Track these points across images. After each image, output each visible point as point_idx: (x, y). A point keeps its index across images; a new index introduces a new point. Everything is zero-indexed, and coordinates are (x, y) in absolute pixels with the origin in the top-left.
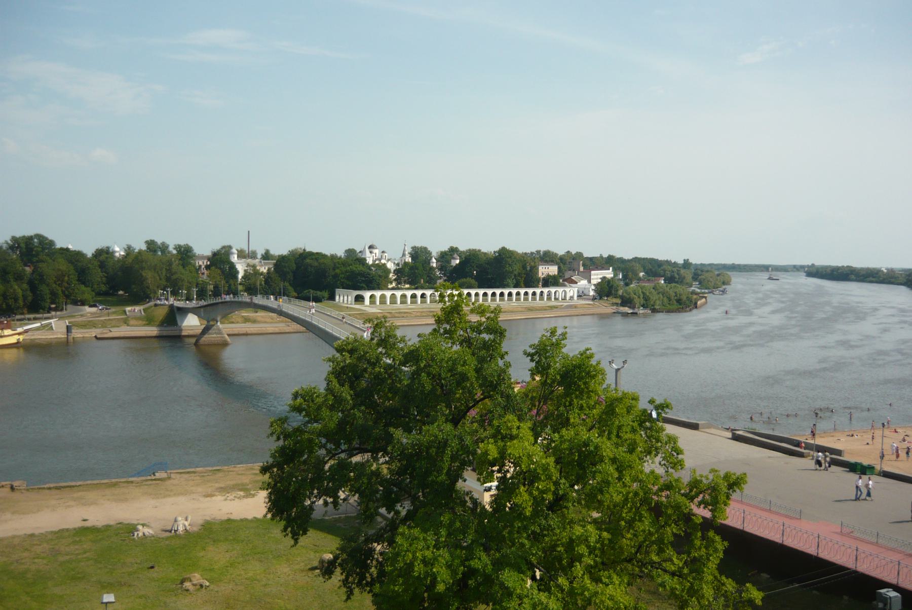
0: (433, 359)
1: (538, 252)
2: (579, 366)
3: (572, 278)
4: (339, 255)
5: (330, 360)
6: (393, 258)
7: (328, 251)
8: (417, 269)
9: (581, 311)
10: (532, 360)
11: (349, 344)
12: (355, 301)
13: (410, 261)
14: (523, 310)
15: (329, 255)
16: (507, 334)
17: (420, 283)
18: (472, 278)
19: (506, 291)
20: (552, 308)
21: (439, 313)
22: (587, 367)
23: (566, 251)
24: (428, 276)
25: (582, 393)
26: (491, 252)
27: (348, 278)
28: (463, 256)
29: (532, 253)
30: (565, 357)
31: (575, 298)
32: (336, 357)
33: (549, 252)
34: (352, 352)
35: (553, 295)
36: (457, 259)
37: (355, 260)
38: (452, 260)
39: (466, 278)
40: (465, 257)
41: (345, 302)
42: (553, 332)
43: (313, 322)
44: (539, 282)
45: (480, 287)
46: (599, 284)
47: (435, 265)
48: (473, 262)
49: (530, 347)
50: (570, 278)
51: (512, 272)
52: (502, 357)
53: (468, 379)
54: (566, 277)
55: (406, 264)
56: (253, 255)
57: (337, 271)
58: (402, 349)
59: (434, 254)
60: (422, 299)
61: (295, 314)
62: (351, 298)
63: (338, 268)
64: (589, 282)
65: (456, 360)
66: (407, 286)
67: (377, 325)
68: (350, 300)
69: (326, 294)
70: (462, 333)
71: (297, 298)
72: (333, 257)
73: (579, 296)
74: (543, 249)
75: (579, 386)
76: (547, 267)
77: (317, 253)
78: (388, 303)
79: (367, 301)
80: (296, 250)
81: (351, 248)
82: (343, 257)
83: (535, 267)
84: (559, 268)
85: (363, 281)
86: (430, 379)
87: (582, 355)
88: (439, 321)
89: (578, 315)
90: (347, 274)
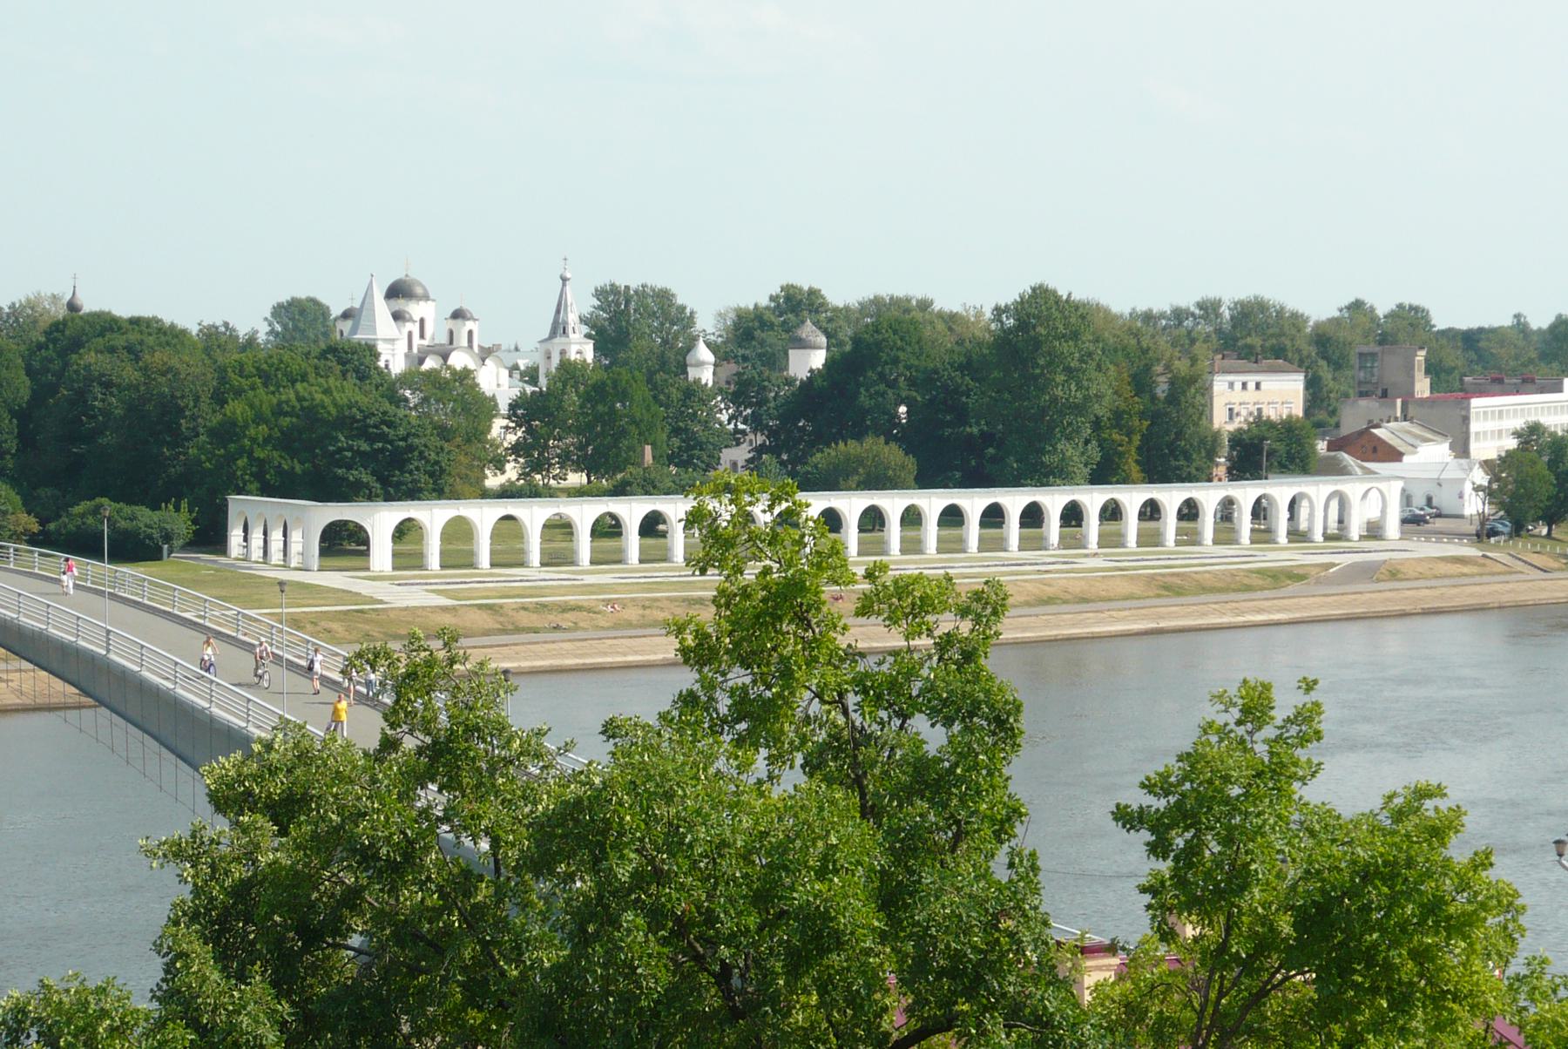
0: (674, 842)
1: (1209, 308)
2: (1386, 872)
3: (1375, 431)
4: (243, 331)
5: (177, 852)
6: (507, 343)
7: (188, 316)
8: (624, 396)
9: (1427, 596)
10: (1158, 848)
11: (273, 771)
12: (324, 552)
13: (589, 355)
14: (1136, 589)
15: (194, 330)
16: (1025, 722)
17: (639, 464)
18: (889, 439)
19: (1053, 501)
20: (1279, 578)
21: (707, 615)
22: (1428, 874)
24: (676, 431)
25: (1402, 1003)
26: (979, 314)
27: (287, 442)
28: (846, 333)
29: (1179, 315)
30: (1324, 826)
31: (1393, 528)
32: (209, 833)
34: (284, 811)
35: (1284, 515)
36: (816, 347)
37: (323, 355)
38: (793, 354)
39: (859, 436)
40: (856, 341)
41: (276, 556)
42: (1255, 708)
43: (113, 656)
44: (1211, 455)
45: (926, 481)
46: (1508, 460)
47: (707, 376)
48: (896, 361)
49: (1148, 786)
50: (1365, 433)
51: (1079, 409)
52: (1002, 829)
53: (838, 941)
54: (1345, 430)
55: (569, 371)
57: (237, 408)
58: (530, 796)
59: (708, 323)
60: (650, 541)
61: (27, 621)
62: (305, 540)
63: (239, 393)
64: (1461, 449)
65: (782, 848)
66: (576, 479)
67: (411, 675)
68: (296, 546)
69: (179, 521)
70: (816, 708)
71: (34, 540)
72: (215, 340)
73: (1412, 521)
74: (1231, 290)
75: (1388, 968)
76: (1251, 379)
77: (135, 321)
78: (484, 559)
80: (31, 304)
81: (302, 294)
82: (262, 337)
83: (1192, 380)
84: (1312, 385)
85: (358, 453)
86: (664, 942)
87: (1399, 815)
88: (699, 654)
89: (1404, 615)
90: (286, 421)
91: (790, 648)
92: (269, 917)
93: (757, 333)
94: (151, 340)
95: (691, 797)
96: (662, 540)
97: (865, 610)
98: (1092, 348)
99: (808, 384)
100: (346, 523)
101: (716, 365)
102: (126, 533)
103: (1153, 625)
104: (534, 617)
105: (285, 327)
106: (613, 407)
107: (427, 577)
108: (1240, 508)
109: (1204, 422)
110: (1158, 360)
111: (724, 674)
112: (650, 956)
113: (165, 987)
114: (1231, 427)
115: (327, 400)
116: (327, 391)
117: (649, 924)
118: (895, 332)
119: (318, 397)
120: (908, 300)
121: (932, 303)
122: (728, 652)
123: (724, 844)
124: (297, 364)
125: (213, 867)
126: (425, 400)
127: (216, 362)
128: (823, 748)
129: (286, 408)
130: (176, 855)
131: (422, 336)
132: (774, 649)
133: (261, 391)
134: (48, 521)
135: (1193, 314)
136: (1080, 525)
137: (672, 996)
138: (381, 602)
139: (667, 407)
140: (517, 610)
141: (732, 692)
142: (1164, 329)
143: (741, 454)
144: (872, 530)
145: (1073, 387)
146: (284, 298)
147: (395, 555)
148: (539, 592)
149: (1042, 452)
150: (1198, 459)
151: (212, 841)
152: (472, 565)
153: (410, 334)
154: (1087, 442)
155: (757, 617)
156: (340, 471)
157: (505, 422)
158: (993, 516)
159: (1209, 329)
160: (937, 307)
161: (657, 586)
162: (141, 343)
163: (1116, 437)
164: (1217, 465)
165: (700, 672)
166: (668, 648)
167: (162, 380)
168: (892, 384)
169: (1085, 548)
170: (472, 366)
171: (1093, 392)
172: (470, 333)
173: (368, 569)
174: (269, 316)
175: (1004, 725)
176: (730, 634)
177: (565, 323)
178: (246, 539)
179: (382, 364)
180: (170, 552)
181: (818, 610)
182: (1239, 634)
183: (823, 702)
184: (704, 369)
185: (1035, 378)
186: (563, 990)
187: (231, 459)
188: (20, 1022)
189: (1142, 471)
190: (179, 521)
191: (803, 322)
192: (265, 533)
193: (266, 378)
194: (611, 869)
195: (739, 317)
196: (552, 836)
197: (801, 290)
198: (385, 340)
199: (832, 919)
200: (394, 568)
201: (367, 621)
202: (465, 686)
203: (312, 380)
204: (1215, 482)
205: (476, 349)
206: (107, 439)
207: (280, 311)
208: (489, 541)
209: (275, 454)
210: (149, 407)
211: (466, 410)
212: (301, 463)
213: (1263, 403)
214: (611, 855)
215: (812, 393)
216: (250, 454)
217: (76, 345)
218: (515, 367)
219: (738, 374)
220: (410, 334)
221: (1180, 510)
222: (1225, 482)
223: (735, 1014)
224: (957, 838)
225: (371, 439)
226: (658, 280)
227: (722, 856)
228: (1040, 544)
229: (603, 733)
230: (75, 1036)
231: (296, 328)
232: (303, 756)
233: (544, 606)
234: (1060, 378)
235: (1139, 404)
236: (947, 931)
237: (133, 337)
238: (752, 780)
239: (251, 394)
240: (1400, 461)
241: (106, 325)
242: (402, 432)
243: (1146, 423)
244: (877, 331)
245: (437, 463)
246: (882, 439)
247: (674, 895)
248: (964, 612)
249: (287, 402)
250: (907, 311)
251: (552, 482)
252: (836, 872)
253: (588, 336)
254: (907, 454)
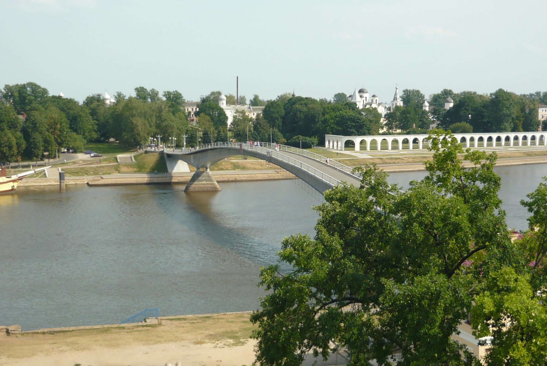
0: (425, 208)
1: (538, 94)
4: (328, 100)
5: (320, 209)
6: (384, 102)
8: (409, 113)
10: (530, 210)
12: (345, 147)
14: (521, 155)
16: (501, 182)
19: (503, 136)
26: (487, 95)
27: (337, 123)
28: (458, 99)
29: (531, 95)
32: (326, 205)
34: (342, 200)
36: (451, 102)
37: (345, 105)
38: (446, 104)
39: (460, 122)
40: (460, 101)
41: (335, 148)
43: (302, 168)
44: (538, 126)
45: (475, 131)
47: (427, 109)
49: (528, 196)
51: (509, 116)
52: (497, 206)
55: (397, 108)
57: (327, 116)
62: (341, 144)
63: (328, 113)
66: (399, 131)
67: (366, 173)
68: (339, 146)
69: (315, 140)
70: (455, 180)
71: (285, 144)
72: (323, 102)
77: (306, 98)
78: (379, 148)
80: (285, 95)
82: (332, 101)
83: (534, 109)
85: (352, 125)
88: (430, 168)
90: (337, 119)
91: (449, 167)
92: (338, 222)
93: (438, 99)
94: (309, 102)
95: (428, 199)
96: (417, 144)
97: (466, 158)
98: (512, 102)
99: (449, 111)
100: (350, 140)
101: (429, 106)
102: (304, 142)
103: (525, 163)
104: (390, 160)
105: (337, 99)
106: (406, 116)
107: (367, 152)
108: (544, 137)
109: (536, 118)
110: (526, 105)
111: (435, 173)
112: (419, 232)
113: (317, 237)
114: (543, 120)
115: (346, 115)
116: (346, 113)
117: (419, 225)
118: (468, 99)
119: (344, 114)
120: (471, 92)
121: (476, 93)
122: (436, 168)
123: (435, 208)
124: (340, 107)
125: (327, 212)
126: (367, 114)
127: (323, 106)
128: (457, 188)
129: (337, 116)
130: (319, 209)
131: (366, 101)
132: (446, 167)
133: (332, 113)
134: (289, 140)
135: (534, 95)
136: (509, 141)
137: (423, 242)
138: (357, 157)
139: (418, 115)
140: (386, 159)
141: (437, 176)
142: (528, 98)
143: (434, 125)
144: (463, 142)
145: (508, 111)
146: (337, 93)
147: (360, 147)
148: (391, 155)
149: (501, 125)
150: (535, 127)
151: (327, 206)
152: (377, 149)
153: (363, 100)
154: (511, 123)
155: (442, 160)
156: (349, 130)
157: (383, 119)
158: (490, 139)
159: (538, 98)
160: (477, 93)
161: (416, 154)
162: (307, 103)
163: (517, 122)
164: (539, 128)
165: (430, 172)
166: (423, 167)
167: (312, 110)
168: (468, 110)
169: (510, 146)
170: (376, 107)
171: (512, 112)
172: (376, 100)
173: (354, 150)
174: (333, 97)
175: (496, 183)
176: (437, 164)
177: (397, 98)
178: (329, 144)
179: (357, 107)
180: (313, 146)
181: (456, 158)
182: (536, 165)
183: (457, 179)
184: (427, 107)
185: (499, 109)
186: (401, 239)
187: (326, 127)
188: (287, 243)
189: (523, 129)
190: (315, 140)
191: (448, 97)
192: (333, 143)
193: (333, 110)
194: (411, 214)
195: (434, 96)
196: (399, 207)
197: (447, 90)
198: (358, 102)
199: (460, 225)
200: (360, 150)
201: (354, 161)
202: (378, 175)
203: (343, 110)
204: (539, 132)
205: (377, 103)
206: (301, 123)
207: (336, 96)
209: (335, 126)
210: (309, 116)
211: (375, 116)
212: (341, 128)
214: (412, 211)
215: (450, 112)
216: (330, 126)
217: (294, 103)
218: (386, 107)
219: (434, 108)
220: (363, 100)
221: (531, 138)
222: (541, 132)
223: (438, 245)
224: (486, 208)
225: (355, 123)
227: (435, 211)
228: (500, 145)
229: (410, 184)
230: (299, 246)
231: (339, 99)
232: (345, 189)
233: (392, 158)
234: (505, 109)
235: (522, 114)
236: (485, 227)
237: (306, 101)
238: (441, 195)
239: (330, 113)
241: (300, 99)
242: (362, 121)
243: (524, 119)
244: (464, 99)
245: (369, 128)
246: (465, 122)
247: (425, 219)
248: (488, 159)
249: (338, 115)
250: (471, 95)
251: (394, 132)
252: (460, 215)
253: (401, 100)
254: (471, 125)
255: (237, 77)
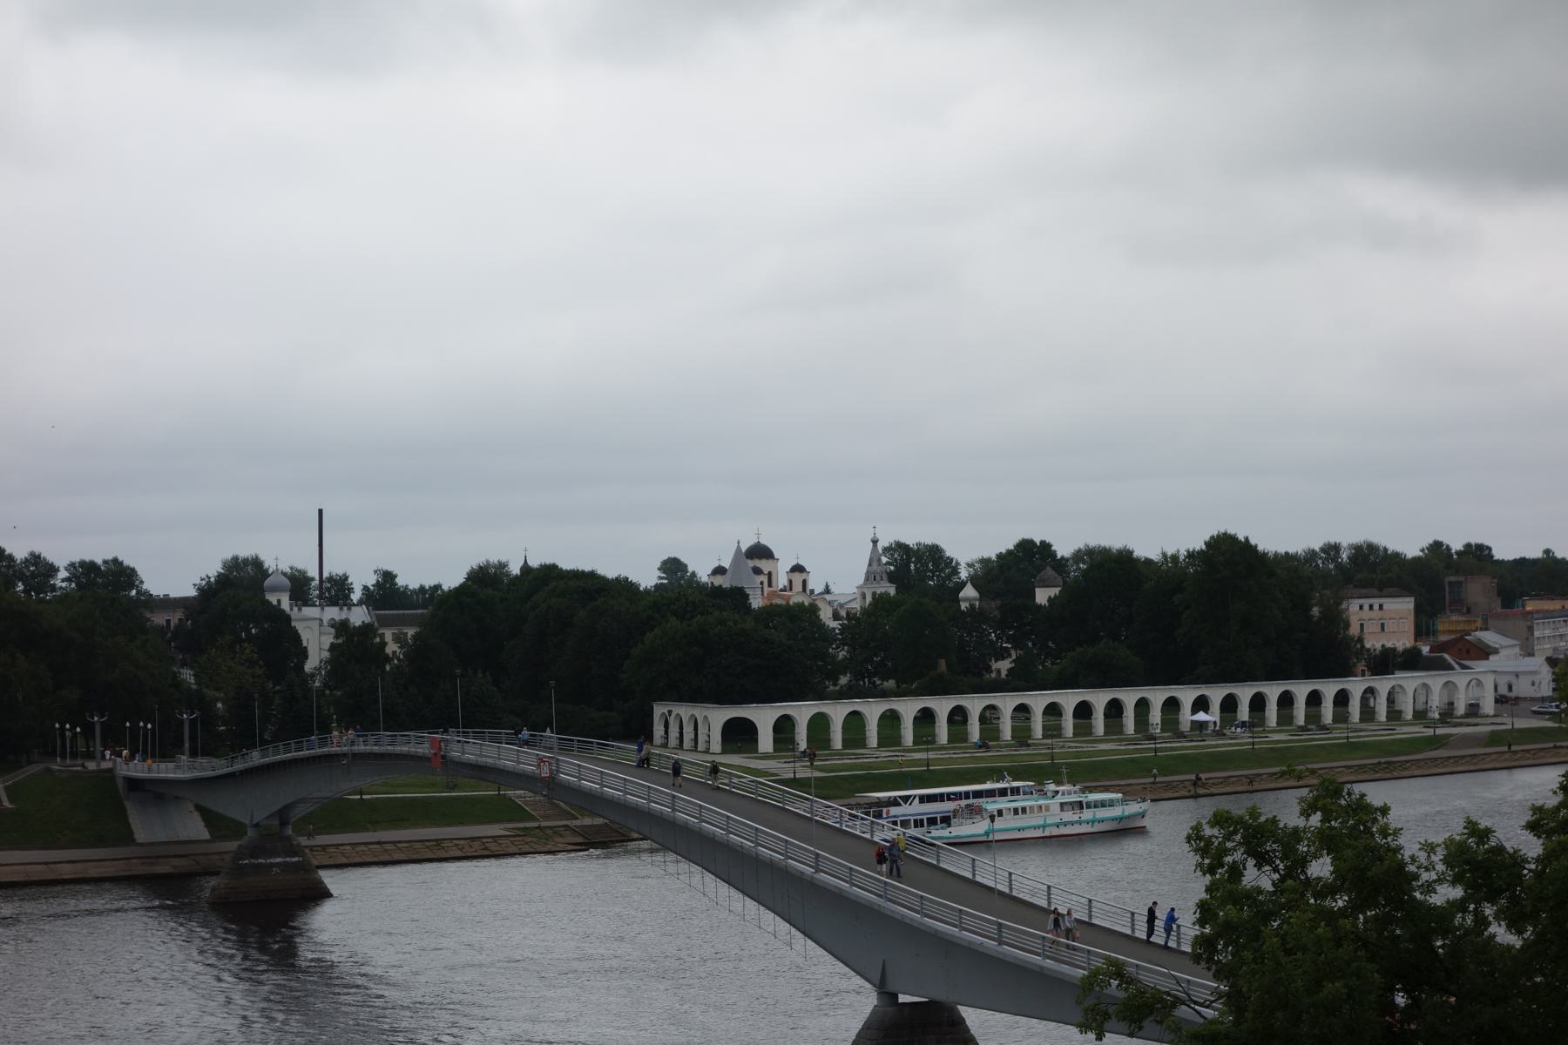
23: (1490, 545)
29: (1312, 555)
31: (1488, 707)
33: (1372, 548)
56: (337, 590)
73: (1500, 700)
74: (1349, 536)
76: (1376, 602)
79: (766, 742)
131: (770, 585)
200: (775, 750)
208: (1276, 708)
213: (1385, 619)
220: (762, 583)
226: (1021, 538)
240: (1488, 659)
255: (320, 512)
